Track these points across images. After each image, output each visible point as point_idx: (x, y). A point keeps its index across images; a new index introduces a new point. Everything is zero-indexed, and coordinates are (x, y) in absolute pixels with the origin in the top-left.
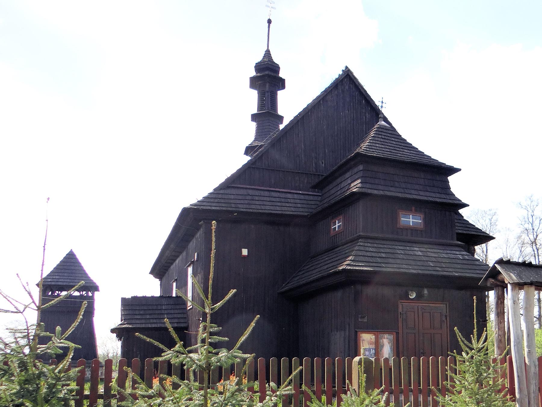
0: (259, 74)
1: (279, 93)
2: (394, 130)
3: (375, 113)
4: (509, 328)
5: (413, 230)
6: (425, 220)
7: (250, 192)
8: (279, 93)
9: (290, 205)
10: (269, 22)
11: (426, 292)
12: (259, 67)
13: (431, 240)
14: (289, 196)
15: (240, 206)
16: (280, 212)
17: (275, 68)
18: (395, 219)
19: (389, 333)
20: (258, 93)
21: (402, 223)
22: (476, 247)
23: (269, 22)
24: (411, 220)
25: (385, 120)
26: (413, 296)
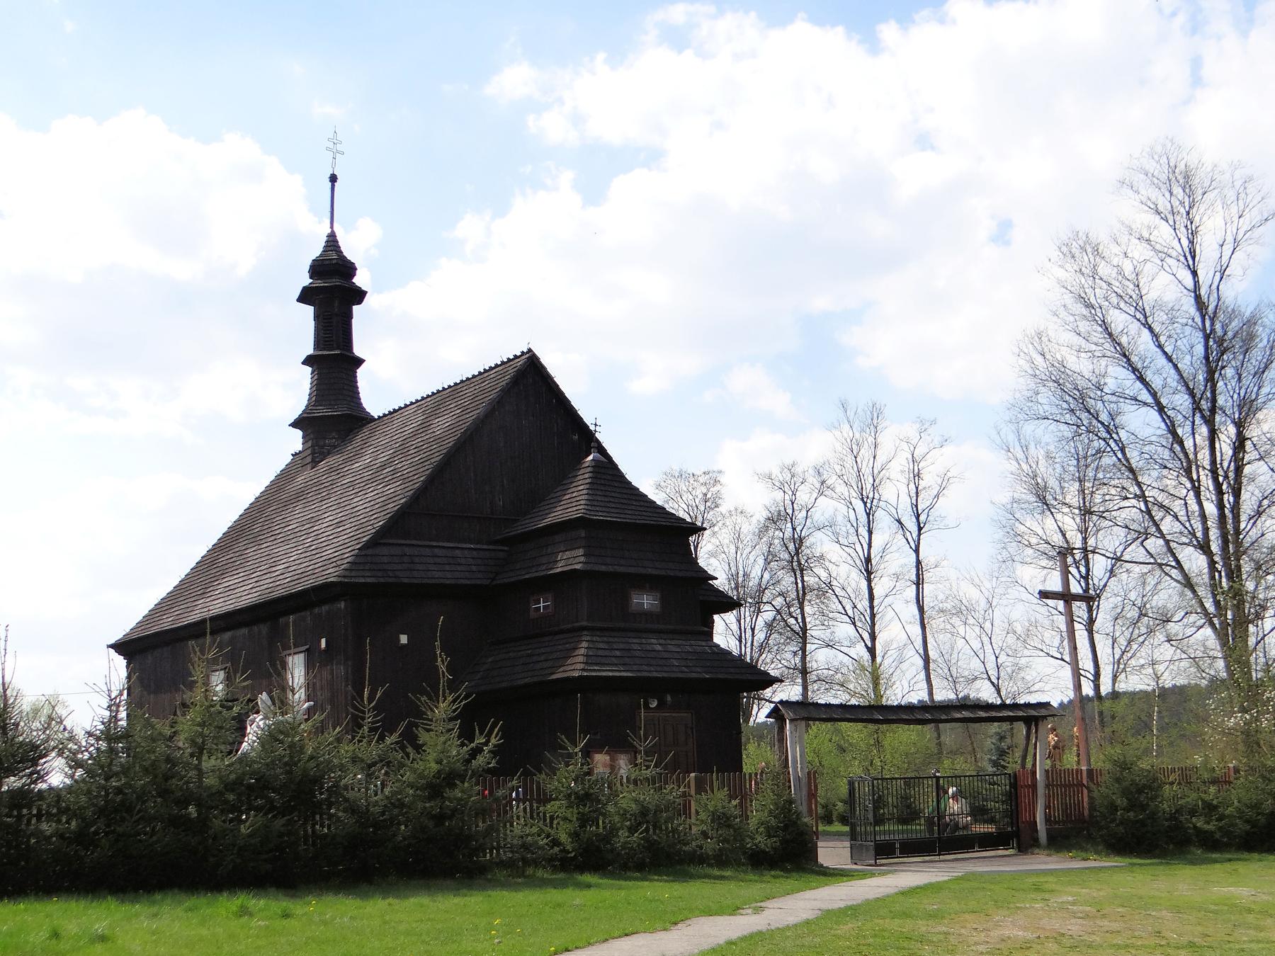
0: (320, 283)
1: (355, 308)
2: (615, 467)
3: (584, 438)
4: (1034, 765)
5: (647, 615)
6: (664, 601)
7: (408, 551)
8: (355, 308)
9: (462, 568)
10: (333, 179)
11: (669, 698)
12: (318, 269)
13: (671, 627)
14: (458, 552)
15: (398, 573)
16: (453, 582)
17: (348, 269)
18: (626, 599)
19: (626, 752)
20: (317, 317)
21: (633, 608)
22: (716, 617)
23: (333, 179)
24: (646, 601)
25: (602, 450)
26: (654, 704)
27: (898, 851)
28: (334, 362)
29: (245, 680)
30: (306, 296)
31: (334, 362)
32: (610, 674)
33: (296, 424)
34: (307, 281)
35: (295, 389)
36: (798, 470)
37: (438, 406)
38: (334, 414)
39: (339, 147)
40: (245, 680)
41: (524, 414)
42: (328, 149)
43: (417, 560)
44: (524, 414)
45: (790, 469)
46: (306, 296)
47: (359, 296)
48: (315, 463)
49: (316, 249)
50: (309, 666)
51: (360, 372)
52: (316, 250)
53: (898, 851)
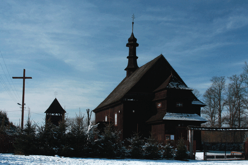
0: (131, 43)
10: (133, 23)
12: (130, 40)
17: (135, 40)
23: (133, 23)
27: (215, 156)
28: (133, 58)
29: (129, 139)
30: (127, 45)
31: (133, 58)
32: (169, 119)
33: (125, 70)
34: (127, 42)
35: (125, 62)
36: (237, 76)
37: (147, 65)
38: (132, 66)
39: (134, 17)
40: (129, 139)
41: (161, 65)
42: (132, 17)
43: (187, 116)
44: (161, 65)
45: (235, 76)
46: (127, 45)
47: (137, 45)
48: (128, 77)
49: (129, 36)
50: (117, 115)
51: (137, 60)
52: (129, 36)
53: (215, 156)
